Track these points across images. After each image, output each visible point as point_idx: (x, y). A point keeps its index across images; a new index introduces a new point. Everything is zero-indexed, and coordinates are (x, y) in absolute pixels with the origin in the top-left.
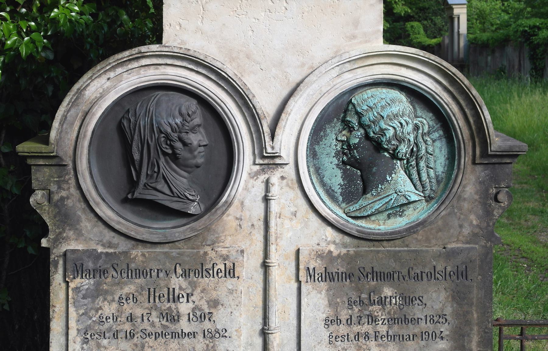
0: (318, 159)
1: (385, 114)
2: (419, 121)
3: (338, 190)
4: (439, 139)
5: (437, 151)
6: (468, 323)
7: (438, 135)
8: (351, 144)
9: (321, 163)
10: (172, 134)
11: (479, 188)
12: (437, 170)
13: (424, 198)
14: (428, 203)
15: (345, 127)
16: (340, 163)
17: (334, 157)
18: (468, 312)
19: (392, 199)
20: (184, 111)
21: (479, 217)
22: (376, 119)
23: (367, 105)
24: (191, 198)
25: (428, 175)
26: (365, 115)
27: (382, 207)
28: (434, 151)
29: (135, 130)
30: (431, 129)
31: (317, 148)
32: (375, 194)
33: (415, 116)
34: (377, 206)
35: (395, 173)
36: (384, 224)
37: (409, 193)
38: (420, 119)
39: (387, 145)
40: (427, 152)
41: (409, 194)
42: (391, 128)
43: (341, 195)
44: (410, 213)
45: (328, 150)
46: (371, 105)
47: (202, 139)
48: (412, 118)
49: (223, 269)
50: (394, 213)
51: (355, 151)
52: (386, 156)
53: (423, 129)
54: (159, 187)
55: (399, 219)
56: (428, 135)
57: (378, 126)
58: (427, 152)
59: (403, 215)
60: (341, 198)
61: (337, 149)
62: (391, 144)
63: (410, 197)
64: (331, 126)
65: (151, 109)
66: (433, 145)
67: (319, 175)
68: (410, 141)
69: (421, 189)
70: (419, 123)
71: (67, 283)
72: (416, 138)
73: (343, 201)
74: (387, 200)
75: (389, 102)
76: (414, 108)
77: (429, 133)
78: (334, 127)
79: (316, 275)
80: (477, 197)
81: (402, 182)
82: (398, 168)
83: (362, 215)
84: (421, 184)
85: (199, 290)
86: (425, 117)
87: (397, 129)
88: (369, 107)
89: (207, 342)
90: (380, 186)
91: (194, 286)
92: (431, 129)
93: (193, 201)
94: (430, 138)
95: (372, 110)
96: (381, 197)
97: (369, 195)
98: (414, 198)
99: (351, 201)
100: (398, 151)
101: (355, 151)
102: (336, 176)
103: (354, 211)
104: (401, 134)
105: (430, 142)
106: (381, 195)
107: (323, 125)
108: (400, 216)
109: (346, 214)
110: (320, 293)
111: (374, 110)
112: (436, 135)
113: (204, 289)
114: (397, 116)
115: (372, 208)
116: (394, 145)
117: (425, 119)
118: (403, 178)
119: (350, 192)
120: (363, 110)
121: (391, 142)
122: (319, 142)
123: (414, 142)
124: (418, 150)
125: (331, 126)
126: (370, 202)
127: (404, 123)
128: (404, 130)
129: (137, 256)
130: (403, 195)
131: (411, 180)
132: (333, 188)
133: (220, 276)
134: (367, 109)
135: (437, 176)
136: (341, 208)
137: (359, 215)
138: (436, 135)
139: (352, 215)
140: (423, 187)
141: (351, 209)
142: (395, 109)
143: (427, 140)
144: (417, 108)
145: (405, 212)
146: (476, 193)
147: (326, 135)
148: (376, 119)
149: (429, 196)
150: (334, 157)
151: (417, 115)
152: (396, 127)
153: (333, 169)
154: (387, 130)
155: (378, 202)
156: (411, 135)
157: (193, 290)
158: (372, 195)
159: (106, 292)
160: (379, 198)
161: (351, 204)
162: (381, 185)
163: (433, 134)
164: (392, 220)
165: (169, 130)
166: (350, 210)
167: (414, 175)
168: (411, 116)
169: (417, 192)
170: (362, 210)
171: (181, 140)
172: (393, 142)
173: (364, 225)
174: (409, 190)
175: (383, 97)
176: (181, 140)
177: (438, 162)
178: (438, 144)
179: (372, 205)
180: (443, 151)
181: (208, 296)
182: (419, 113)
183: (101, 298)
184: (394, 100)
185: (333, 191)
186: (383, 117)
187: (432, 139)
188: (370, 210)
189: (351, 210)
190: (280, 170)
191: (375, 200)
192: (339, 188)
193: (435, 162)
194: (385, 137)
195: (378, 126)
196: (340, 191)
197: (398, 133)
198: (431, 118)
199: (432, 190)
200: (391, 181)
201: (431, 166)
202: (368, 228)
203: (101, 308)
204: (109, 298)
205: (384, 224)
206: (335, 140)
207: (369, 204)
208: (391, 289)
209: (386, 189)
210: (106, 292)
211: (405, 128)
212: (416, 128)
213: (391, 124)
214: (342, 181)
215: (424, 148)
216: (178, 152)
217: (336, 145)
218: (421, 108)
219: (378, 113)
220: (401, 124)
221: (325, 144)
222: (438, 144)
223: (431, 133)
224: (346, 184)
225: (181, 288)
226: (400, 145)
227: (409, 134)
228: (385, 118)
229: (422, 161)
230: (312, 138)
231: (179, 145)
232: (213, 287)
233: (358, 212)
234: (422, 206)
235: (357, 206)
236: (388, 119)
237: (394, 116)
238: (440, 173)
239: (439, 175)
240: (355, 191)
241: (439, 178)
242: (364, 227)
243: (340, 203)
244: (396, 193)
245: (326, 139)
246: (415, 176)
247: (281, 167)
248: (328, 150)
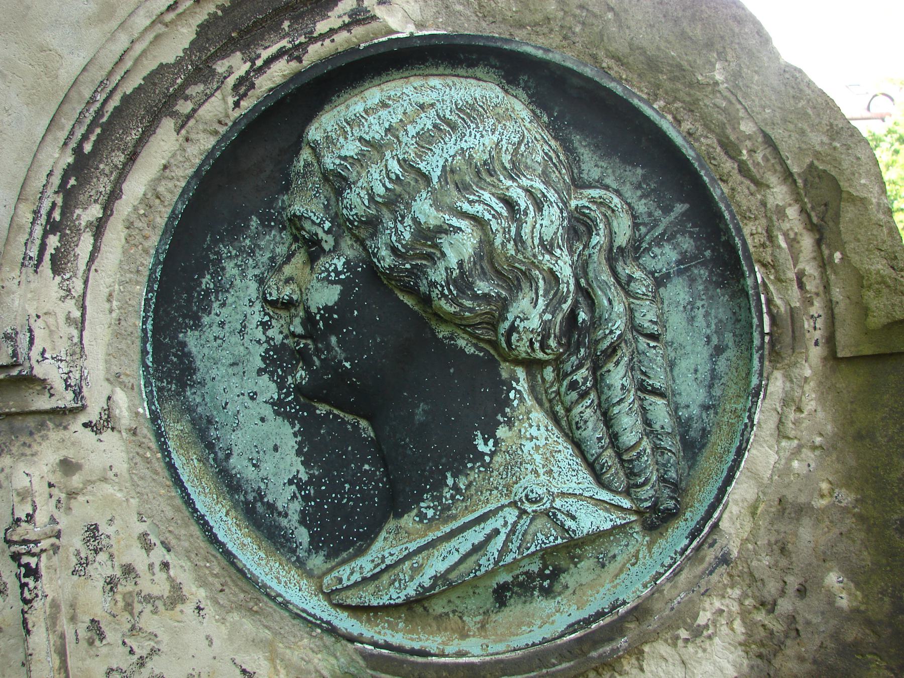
0: (202, 384)
1: (433, 165)
2: (593, 200)
4: (680, 273)
5: (676, 320)
7: (674, 256)
8: (314, 310)
9: (213, 398)
11: (853, 463)
12: (683, 400)
13: (633, 518)
14: (655, 534)
15: (293, 248)
16: (288, 394)
17: (260, 372)
19: (496, 532)
22: (398, 189)
23: (361, 139)
25: (647, 423)
26: (353, 176)
27: (462, 568)
28: (661, 321)
30: (643, 230)
31: (191, 339)
32: (430, 513)
33: (573, 179)
35: (510, 423)
36: (483, 626)
37: (571, 500)
38: (595, 193)
39: (454, 301)
40: (634, 327)
41: (571, 505)
42: (463, 224)
43: (302, 522)
44: (586, 578)
48: (561, 185)
50: (521, 585)
51: (333, 340)
52: (462, 351)
53: (611, 235)
55: (542, 605)
56: (636, 259)
57: (408, 221)
58: (634, 327)
59: (558, 588)
60: (303, 536)
61: (269, 340)
62: (475, 297)
63: (573, 518)
64: (241, 251)
66: (656, 298)
67: (210, 446)
68: (557, 279)
69: (620, 482)
70: (594, 207)
72: (581, 268)
73: (315, 545)
74: (475, 536)
75: (453, 118)
76: (569, 149)
77: (635, 250)
78: (252, 253)
80: (847, 498)
81: (538, 458)
82: (522, 400)
83: (385, 600)
84: (622, 461)
86: (614, 185)
87: (494, 225)
88: (367, 143)
90: (450, 481)
92: (643, 230)
94: (642, 268)
95: (383, 156)
96: (455, 525)
97: (408, 521)
99: (345, 545)
100: (507, 325)
101: (333, 340)
102: (276, 449)
103: (356, 584)
104: (510, 246)
106: (454, 518)
107: (209, 248)
108: (547, 593)
111: (388, 154)
114: (491, 173)
115: (417, 570)
116: (486, 297)
117: (618, 192)
118: (541, 443)
119: (337, 508)
120: (345, 158)
121: (470, 286)
122: (199, 318)
123: (577, 283)
124: (596, 322)
125: (241, 251)
126: (413, 546)
127: (523, 201)
128: (526, 230)
130: (546, 513)
131: (578, 446)
132: (269, 498)
134: (362, 154)
135: (683, 425)
136: (309, 574)
137: (374, 603)
139: (349, 602)
140: (631, 474)
141: (345, 578)
143: (630, 278)
144: (581, 150)
145: (564, 578)
146: (847, 481)
147: (220, 288)
148: (398, 189)
149: (654, 508)
150: (260, 372)
151: (584, 176)
152: (487, 216)
153: (263, 420)
154: (446, 232)
156: (558, 252)
158: (422, 516)
160: (447, 529)
161: (345, 555)
162: (454, 476)
163: (657, 250)
164: (515, 610)
166: (340, 580)
167: (590, 425)
168: (554, 176)
169: (604, 495)
170: (385, 579)
172: (482, 287)
173: (397, 639)
174: (571, 486)
175: (427, 100)
177: (684, 365)
179: (419, 558)
180: (700, 321)
182: (591, 166)
184: (473, 108)
185: (271, 507)
186: (427, 178)
187: (652, 273)
188: (412, 579)
189: (345, 583)
190: (55, 435)
191: (431, 536)
192: (294, 497)
193: (672, 365)
194: (441, 265)
195: (408, 221)
196: (297, 506)
197: (498, 241)
198: (639, 187)
199: (665, 481)
200: (492, 454)
201: (657, 385)
202: (413, 652)
205: (483, 626)
206: (258, 306)
207: (409, 556)
209: (473, 489)
211: (530, 219)
213: (466, 207)
214: (302, 469)
215: (619, 308)
217: (265, 326)
218: (597, 147)
219: (403, 163)
221: (222, 324)
223: (647, 250)
224: (319, 478)
226: (514, 298)
227: (548, 247)
228: (435, 180)
229: (617, 364)
233: (371, 588)
234: (631, 549)
235: (366, 564)
236: (451, 186)
237: (478, 173)
238: (695, 411)
239: (690, 418)
240: (356, 506)
241: (692, 433)
242: (400, 649)
243: (302, 554)
244: (514, 504)
245: (223, 305)
246: (595, 430)
247: (57, 426)
248: (235, 346)
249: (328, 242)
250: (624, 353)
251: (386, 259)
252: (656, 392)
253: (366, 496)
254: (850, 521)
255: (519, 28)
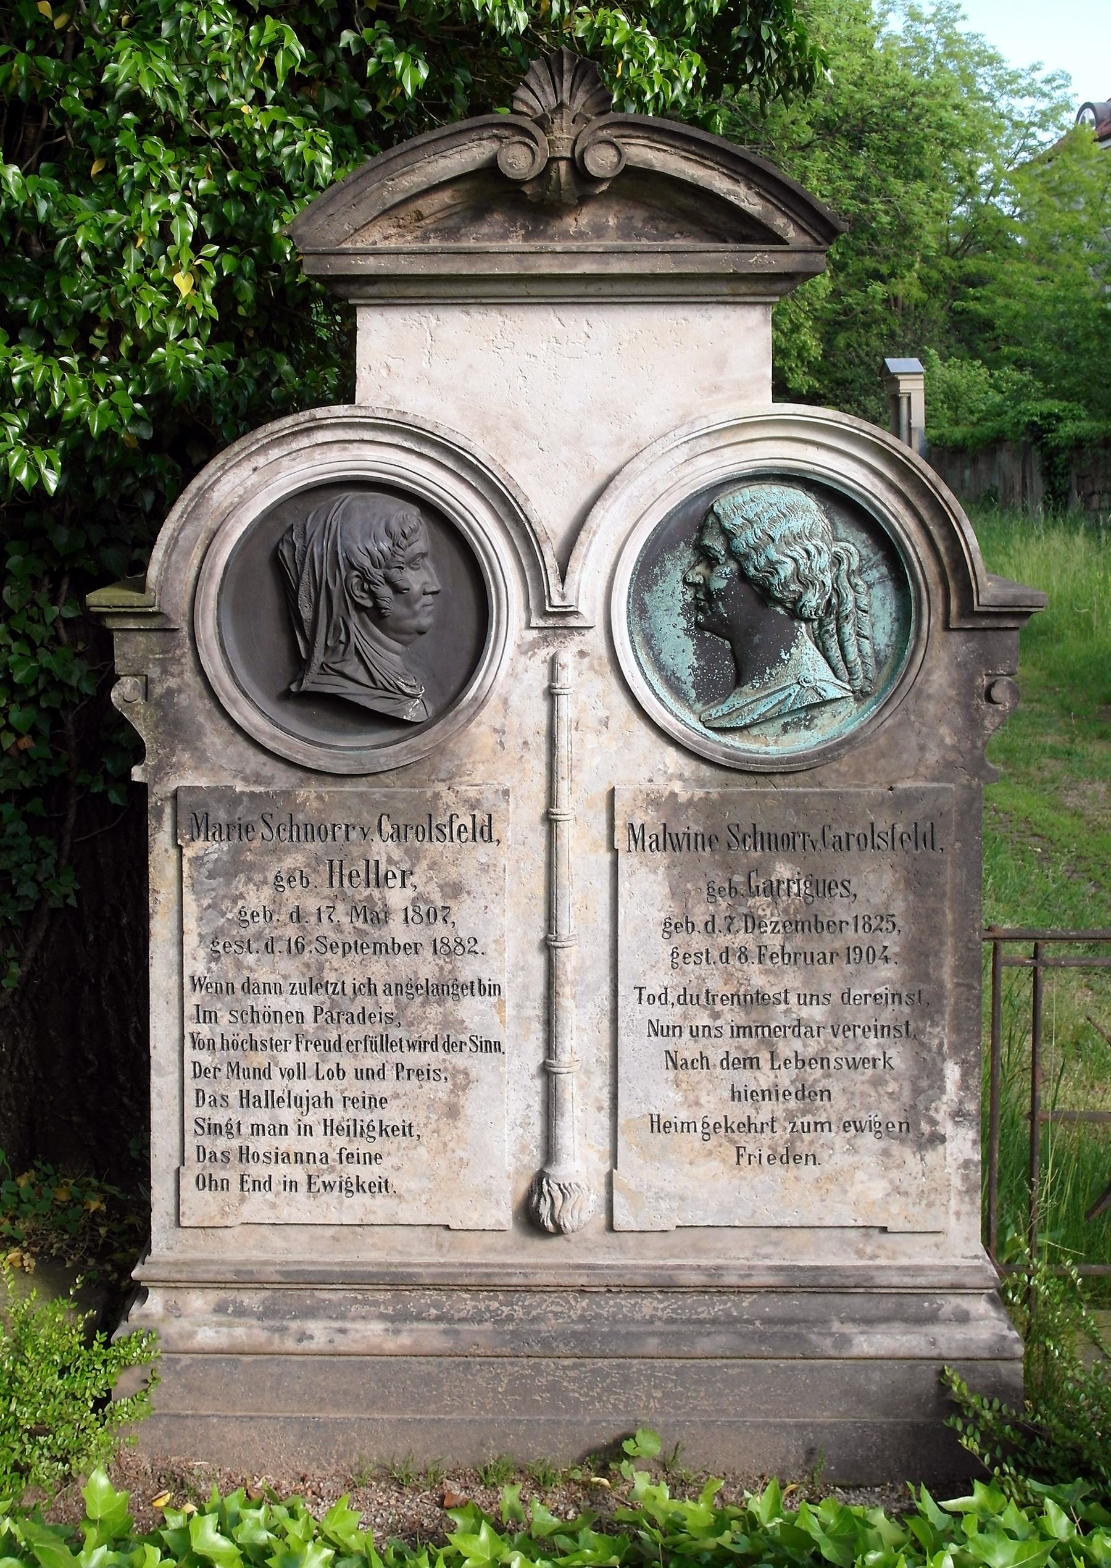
3: (687, 678)
5: (876, 604)
6: (935, 931)
10: (373, 570)
18: (935, 911)
20: (395, 528)
21: (956, 731)
24: (408, 690)
25: (860, 651)
29: (303, 563)
31: (647, 597)
34: (762, 708)
38: (843, 544)
42: (788, 560)
44: (826, 722)
45: (669, 602)
46: (751, 515)
47: (429, 580)
49: (470, 826)
53: (849, 564)
54: (348, 670)
55: (804, 734)
58: (858, 607)
60: (693, 694)
65: (334, 524)
66: (868, 594)
67: (651, 648)
69: (846, 677)
71: (180, 848)
72: (836, 579)
73: (698, 699)
76: (833, 523)
77: (860, 571)
79: (647, 838)
80: (952, 693)
85: (424, 864)
89: (441, 962)
91: (415, 856)
93: (413, 697)
97: (747, 688)
98: (832, 693)
105: (862, 586)
108: (807, 728)
109: (703, 723)
110: (655, 872)
112: (874, 575)
113: (435, 863)
115: (752, 711)
119: (711, 681)
127: (813, 551)
129: (307, 799)
133: (463, 838)
136: (694, 712)
138: (874, 575)
142: (796, 524)
145: (816, 721)
149: (861, 691)
155: (764, 701)
157: (413, 865)
159: (252, 866)
165: (367, 563)
169: (838, 682)
171: (389, 581)
172: (793, 587)
173: (737, 744)
176: (389, 581)
177: (879, 625)
178: (878, 591)
180: (888, 606)
181: (442, 875)
182: (842, 532)
183: (242, 877)
185: (678, 679)
190: (577, 638)
193: (873, 625)
196: (692, 679)
203: (242, 896)
204: (257, 877)
208: (790, 866)
210: (252, 866)
212: (837, 560)
215: (851, 598)
216: (384, 604)
220: (807, 552)
222: (878, 591)
225: (390, 860)
227: (822, 572)
230: (638, 578)
231: (385, 591)
232: (451, 859)
242: (738, 749)
249: (722, 560)
250: (852, 618)
251: (752, 571)
252: (865, 637)
253: (725, 676)
254: (952, 704)
255: (979, 1523)
